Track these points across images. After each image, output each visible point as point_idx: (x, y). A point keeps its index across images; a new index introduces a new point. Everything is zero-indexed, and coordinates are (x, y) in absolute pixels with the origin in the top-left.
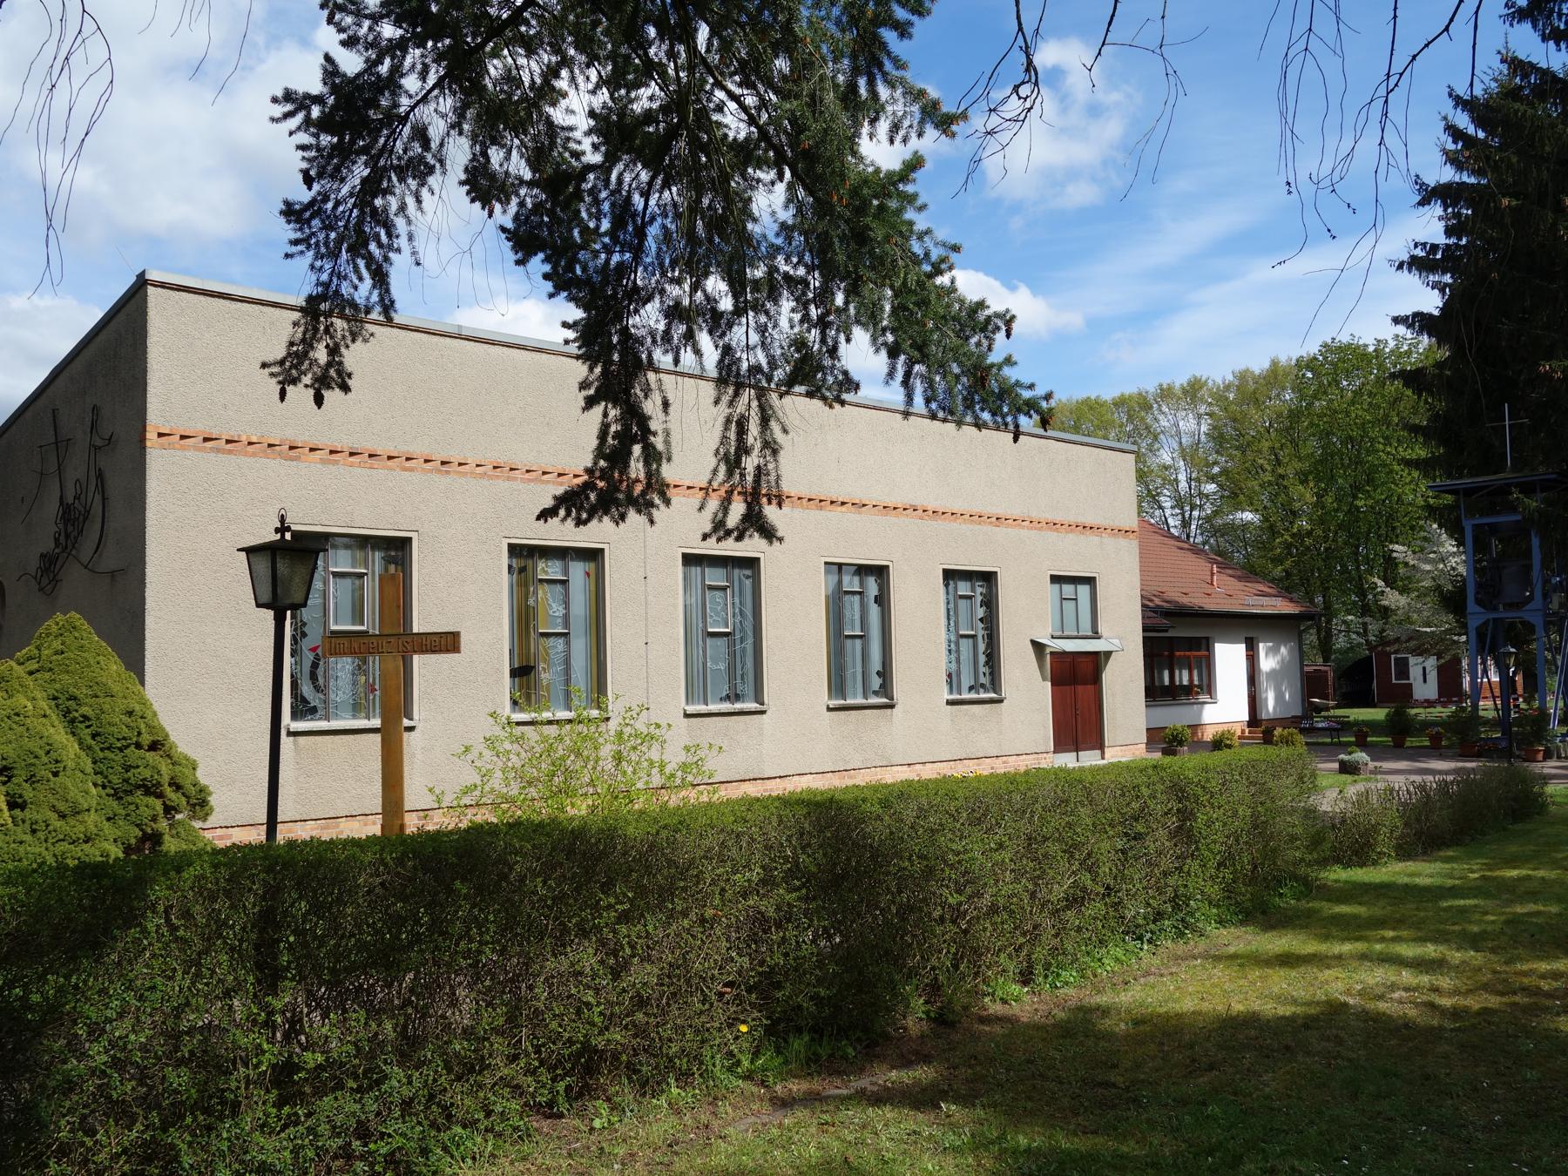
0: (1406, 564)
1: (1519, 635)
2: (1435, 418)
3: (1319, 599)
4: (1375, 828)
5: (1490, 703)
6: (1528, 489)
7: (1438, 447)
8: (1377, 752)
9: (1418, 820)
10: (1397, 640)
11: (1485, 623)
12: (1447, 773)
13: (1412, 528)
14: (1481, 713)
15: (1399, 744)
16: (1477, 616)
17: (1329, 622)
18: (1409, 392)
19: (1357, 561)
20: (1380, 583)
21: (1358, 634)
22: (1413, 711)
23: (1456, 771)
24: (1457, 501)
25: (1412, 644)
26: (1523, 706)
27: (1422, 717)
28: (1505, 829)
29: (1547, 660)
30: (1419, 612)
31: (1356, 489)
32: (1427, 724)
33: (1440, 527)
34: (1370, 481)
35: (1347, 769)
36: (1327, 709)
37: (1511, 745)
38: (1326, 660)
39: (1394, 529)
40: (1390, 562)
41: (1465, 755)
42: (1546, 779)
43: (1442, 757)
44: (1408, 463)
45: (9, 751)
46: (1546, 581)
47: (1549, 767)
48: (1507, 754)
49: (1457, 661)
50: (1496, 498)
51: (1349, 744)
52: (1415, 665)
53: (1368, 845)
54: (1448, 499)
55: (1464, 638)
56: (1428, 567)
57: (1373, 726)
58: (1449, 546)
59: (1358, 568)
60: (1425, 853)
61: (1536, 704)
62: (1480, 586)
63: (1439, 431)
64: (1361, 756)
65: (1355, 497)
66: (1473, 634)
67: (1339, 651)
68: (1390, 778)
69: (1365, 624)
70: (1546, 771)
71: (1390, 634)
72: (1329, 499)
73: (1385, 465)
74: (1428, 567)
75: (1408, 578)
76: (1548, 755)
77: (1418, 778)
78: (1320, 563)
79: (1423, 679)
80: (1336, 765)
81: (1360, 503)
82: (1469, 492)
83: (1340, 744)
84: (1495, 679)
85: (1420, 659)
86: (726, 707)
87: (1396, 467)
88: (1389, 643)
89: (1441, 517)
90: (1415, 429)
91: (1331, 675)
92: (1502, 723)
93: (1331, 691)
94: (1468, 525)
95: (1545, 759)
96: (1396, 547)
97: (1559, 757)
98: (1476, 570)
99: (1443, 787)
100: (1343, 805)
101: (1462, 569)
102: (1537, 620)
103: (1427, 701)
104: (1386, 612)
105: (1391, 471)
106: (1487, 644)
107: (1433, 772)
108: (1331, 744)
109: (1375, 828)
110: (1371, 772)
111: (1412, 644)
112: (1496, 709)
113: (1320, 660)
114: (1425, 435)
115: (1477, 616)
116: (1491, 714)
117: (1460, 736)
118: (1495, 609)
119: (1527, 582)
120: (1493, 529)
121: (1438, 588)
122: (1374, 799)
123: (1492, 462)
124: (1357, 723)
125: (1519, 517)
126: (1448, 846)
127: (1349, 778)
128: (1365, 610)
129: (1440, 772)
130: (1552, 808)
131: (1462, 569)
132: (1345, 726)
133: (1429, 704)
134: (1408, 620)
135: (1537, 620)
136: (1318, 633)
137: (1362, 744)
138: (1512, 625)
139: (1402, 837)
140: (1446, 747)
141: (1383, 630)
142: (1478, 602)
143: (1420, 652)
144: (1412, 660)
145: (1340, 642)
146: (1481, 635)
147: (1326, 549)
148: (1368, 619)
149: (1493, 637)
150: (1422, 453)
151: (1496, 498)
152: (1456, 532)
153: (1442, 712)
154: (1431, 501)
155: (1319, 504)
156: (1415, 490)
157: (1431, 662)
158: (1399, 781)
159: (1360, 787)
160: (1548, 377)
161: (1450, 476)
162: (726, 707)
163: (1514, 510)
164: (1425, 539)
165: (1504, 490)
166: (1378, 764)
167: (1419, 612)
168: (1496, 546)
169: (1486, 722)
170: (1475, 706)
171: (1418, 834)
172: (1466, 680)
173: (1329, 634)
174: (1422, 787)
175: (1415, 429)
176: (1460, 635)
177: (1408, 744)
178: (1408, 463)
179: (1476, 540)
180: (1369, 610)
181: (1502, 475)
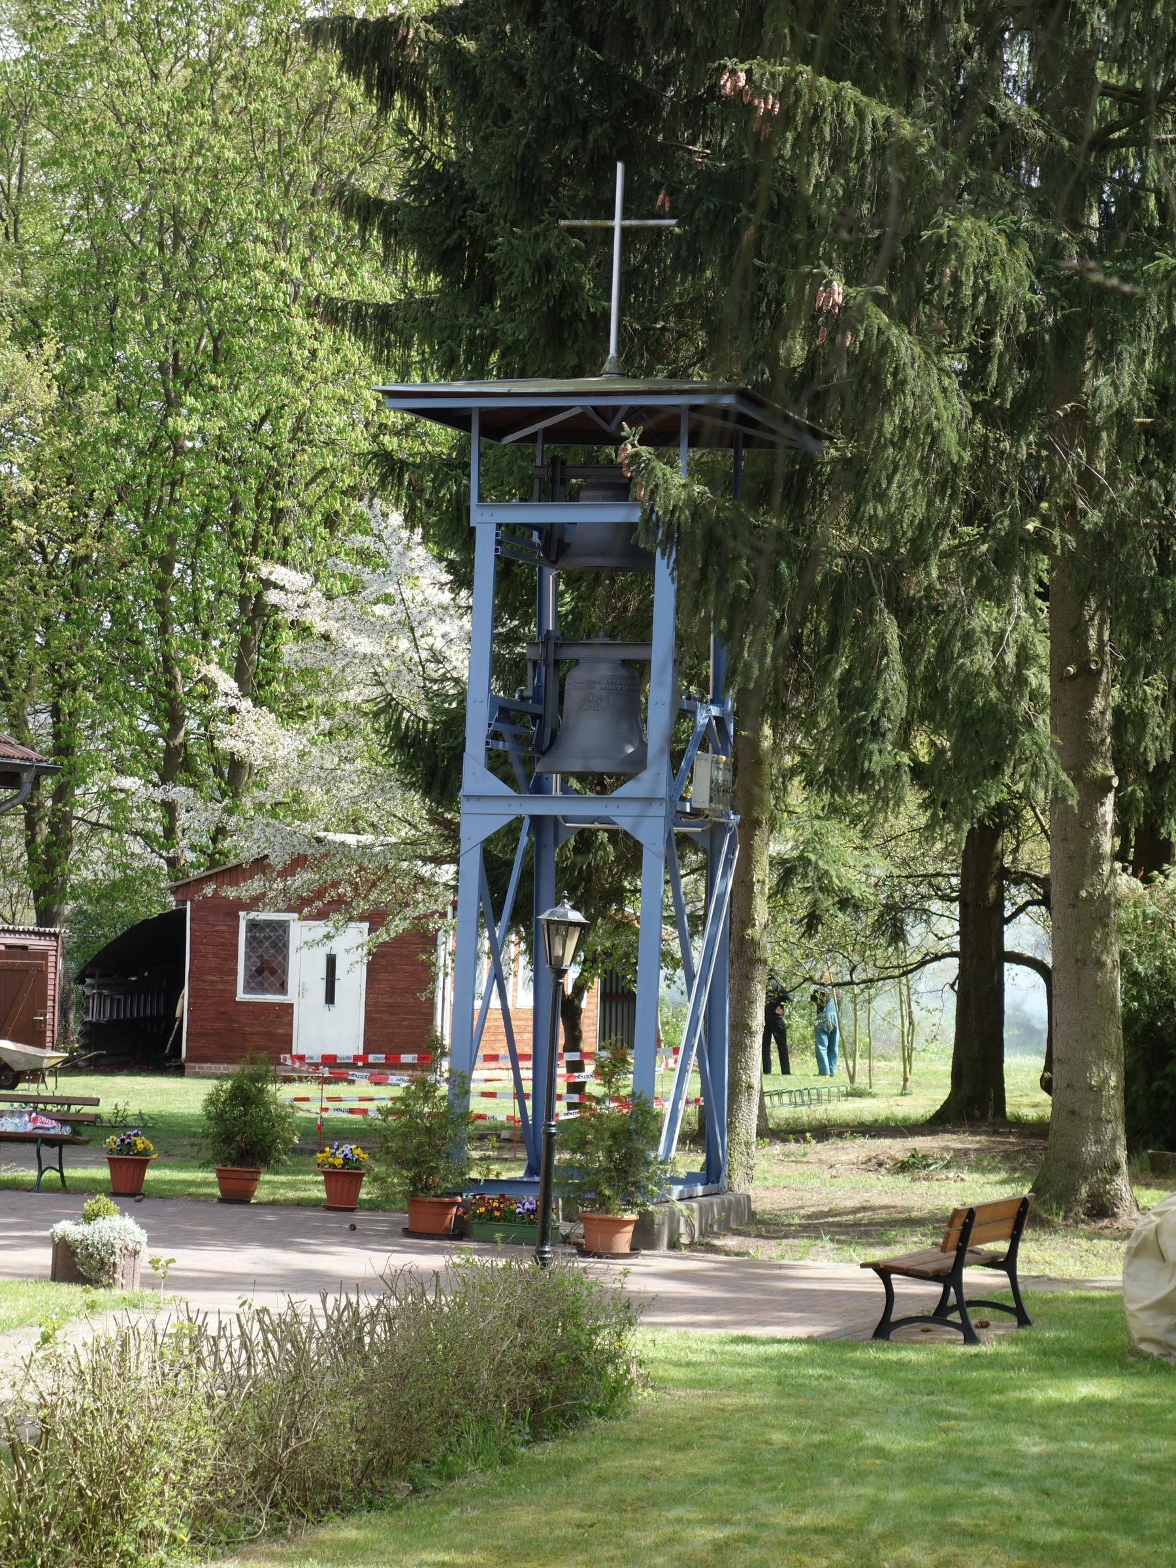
0: (303, 630)
1: (596, 875)
2: (430, 181)
3: (40, 723)
4: (135, 1457)
5: (503, 1078)
6: (661, 433)
7: (423, 271)
8: (171, 1216)
9: (265, 1431)
10: (260, 864)
11: (511, 831)
12: (361, 1286)
13: (331, 521)
14: (477, 1105)
15: (236, 1195)
16: (487, 804)
17: (61, 794)
18: (355, 90)
19: (161, 605)
20: (226, 683)
21: (147, 837)
22: (285, 1093)
23: (390, 1283)
24: (463, 449)
25: (302, 880)
26: (594, 1087)
27: (311, 1110)
28: (506, 1461)
29: (666, 957)
30: (329, 781)
31: (180, 376)
32: (321, 1135)
33: (411, 520)
34: (219, 356)
35: (75, 1266)
36: (36, 1075)
37: (546, 1201)
38: (46, 917)
39: (278, 515)
40: (257, 613)
41: (419, 1232)
42: (629, 1309)
43: (354, 1235)
44: (333, 312)
45: (1146, 1203)
46: (683, 714)
47: (645, 1273)
48: (537, 1231)
49: (424, 939)
50: (572, 451)
51: (88, 1189)
52: (307, 946)
53: (113, 1507)
54: (440, 438)
55: (447, 872)
56: (365, 645)
57: (168, 1135)
58: (424, 577)
59: (164, 629)
60: (276, 1532)
61: (627, 1084)
62: (504, 713)
63: (435, 220)
64: (117, 1227)
65: (172, 403)
66: (472, 860)
67: (84, 889)
68: (199, 1300)
69: (169, 808)
70: (634, 1285)
71: (242, 846)
72: (96, 401)
73: (264, 311)
74: (365, 645)
75: (306, 672)
76: (645, 1237)
77: (277, 1303)
78: (55, 608)
79: (324, 998)
80: (44, 1257)
81: (184, 424)
82: (496, 424)
83: (64, 1187)
84: (522, 997)
85: (320, 929)
86: (607, 641)
87: (300, 324)
88: (236, 874)
89: (416, 491)
90: (362, 209)
91: (56, 970)
92: (533, 1138)
93: (51, 1016)
94: (486, 521)
95: (635, 1248)
96: (280, 574)
97: (674, 1245)
98: (498, 666)
99: (347, 1335)
100: (47, 1382)
101: (459, 661)
102: (652, 835)
103: (329, 1060)
104: (234, 772)
105: (285, 334)
106: (511, 891)
107: (319, 1282)
108: (38, 1187)
109: (135, 1457)
110: (149, 1282)
111: (302, 880)
112: (520, 1095)
113: (28, 918)
114: (388, 231)
115: (487, 804)
116: (503, 1110)
117: (416, 1177)
118: (539, 788)
119: (631, 711)
120: (555, 542)
121: (389, 706)
122: (142, 1363)
123: (565, 337)
124: (119, 1124)
125: (636, 516)
126: (346, 1512)
127: (72, 1294)
128: (175, 765)
129: (341, 1284)
130: (643, 1396)
131: (459, 661)
132: (79, 1131)
133: (335, 1069)
134: (293, 805)
135: (652, 835)
136: (31, 825)
137: (128, 1186)
138: (585, 840)
139: (213, 1483)
140: (373, 1206)
141: (220, 832)
142: (496, 763)
143: (323, 905)
144: (300, 931)
145: (90, 865)
146: (494, 869)
147: (76, 562)
148: (179, 793)
149: (528, 876)
150: (381, 288)
151: (572, 451)
152: (451, 533)
153: (370, 1097)
154: (390, 442)
155: (66, 413)
156: (349, 399)
157: (352, 943)
158: (220, 1309)
159: (106, 1326)
160: (739, 106)
161: (449, 366)
162: (607, 641)
163: (621, 490)
164: (364, 556)
165: (592, 429)
166: (164, 1253)
167: (329, 781)
168: (557, 599)
169: (489, 1134)
170: (461, 1082)
171: (265, 1473)
172: (445, 993)
173: (61, 839)
174: (286, 1329)
175: (362, 209)
176: (437, 860)
177: (261, 1193)
178: (333, 312)
179: (505, 572)
180: (188, 765)
181: (590, 383)
